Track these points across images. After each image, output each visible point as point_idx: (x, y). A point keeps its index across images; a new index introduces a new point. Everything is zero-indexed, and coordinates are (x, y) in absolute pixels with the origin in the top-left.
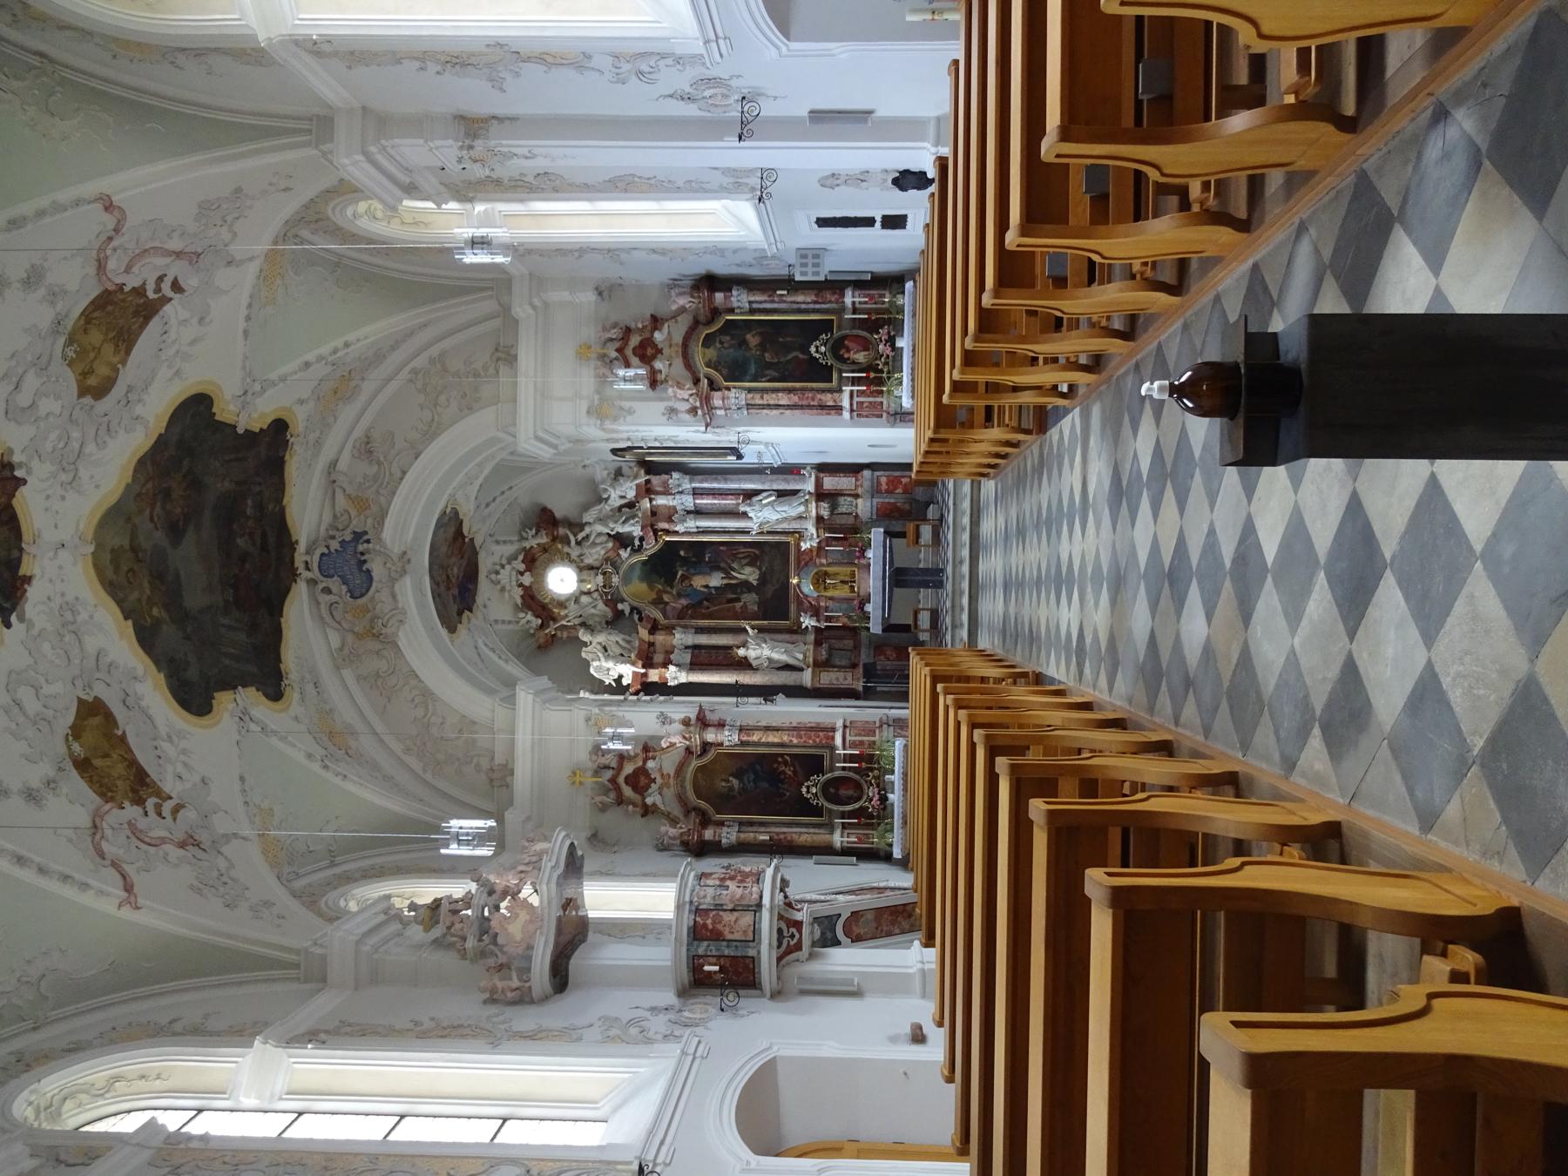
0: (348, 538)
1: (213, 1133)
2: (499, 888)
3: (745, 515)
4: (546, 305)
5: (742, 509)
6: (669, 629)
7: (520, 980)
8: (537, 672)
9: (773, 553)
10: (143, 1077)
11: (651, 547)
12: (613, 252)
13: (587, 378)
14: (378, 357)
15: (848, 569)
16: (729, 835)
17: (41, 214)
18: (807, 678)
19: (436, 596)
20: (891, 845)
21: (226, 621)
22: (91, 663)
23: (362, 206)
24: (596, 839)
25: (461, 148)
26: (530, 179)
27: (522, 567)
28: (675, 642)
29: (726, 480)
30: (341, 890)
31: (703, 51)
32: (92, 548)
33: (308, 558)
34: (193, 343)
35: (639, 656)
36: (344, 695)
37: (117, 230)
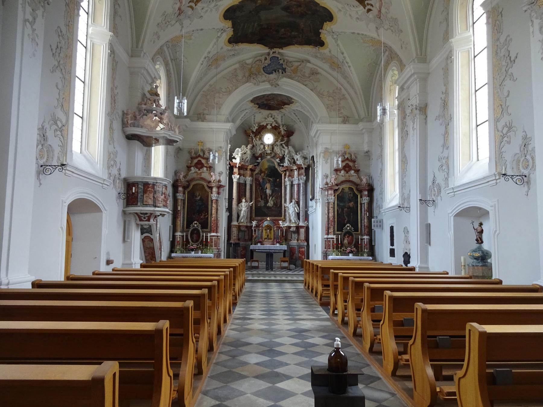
2: (163, 116)
3: (291, 202)
4: (363, 134)
5: (293, 201)
6: (252, 175)
7: (131, 124)
8: (237, 130)
9: (278, 211)
11: (280, 169)
12: (381, 157)
13: (338, 148)
14: (345, 77)
15: (272, 237)
16: (180, 196)
18: (235, 223)
19: (263, 96)
20: (176, 253)
21: (256, 25)
24: (179, 150)
25: (416, 106)
26: (406, 129)
27: (273, 125)
28: (247, 177)
29: (303, 195)
33: (277, 52)
34: (350, 15)
35: (242, 165)
36: (230, 64)
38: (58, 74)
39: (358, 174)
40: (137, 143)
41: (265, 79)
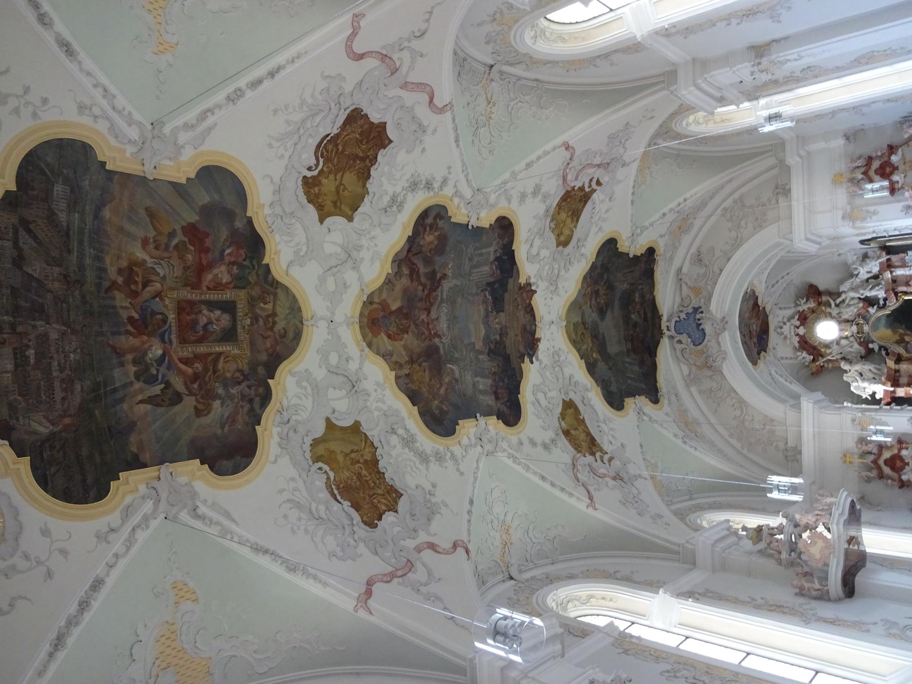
0: (690, 311)
1: (643, 636)
4: (808, 153)
7: (821, 585)
8: (812, 390)
10: (603, 598)
11: (893, 304)
12: (857, 109)
13: (841, 195)
14: (703, 204)
17: (539, 158)
19: (744, 343)
21: (627, 360)
22: (567, 381)
23: (691, 118)
25: (753, 66)
26: (798, 74)
27: (798, 323)
30: (698, 514)
32: (565, 323)
33: (668, 324)
34: (607, 211)
35: (888, 379)
36: (693, 401)
37: (571, 159)
39: (897, 147)
41: (714, 341)
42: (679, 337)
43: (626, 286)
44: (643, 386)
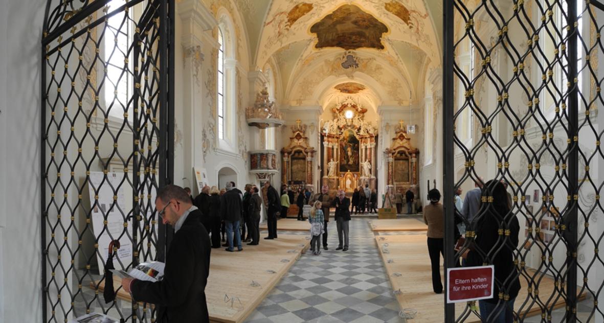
0: (357, 62)
3: (366, 161)
5: (367, 160)
9: (356, 168)
11: (357, 137)
18: (325, 177)
21: (334, 34)
22: (322, 5)
31: (531, 127)
32: (349, 4)
34: (399, 29)
38: (210, 97)
40: (255, 127)
42: (346, 57)
43: (367, 34)
44: (323, 41)
